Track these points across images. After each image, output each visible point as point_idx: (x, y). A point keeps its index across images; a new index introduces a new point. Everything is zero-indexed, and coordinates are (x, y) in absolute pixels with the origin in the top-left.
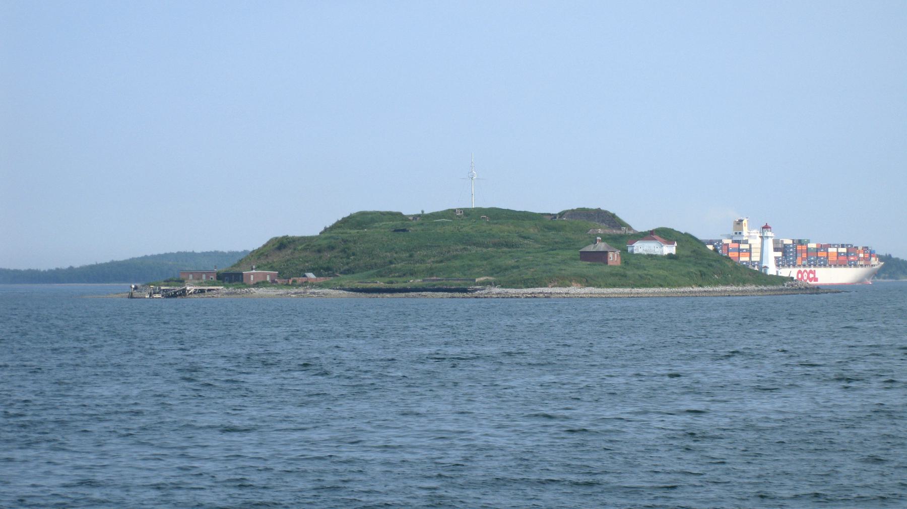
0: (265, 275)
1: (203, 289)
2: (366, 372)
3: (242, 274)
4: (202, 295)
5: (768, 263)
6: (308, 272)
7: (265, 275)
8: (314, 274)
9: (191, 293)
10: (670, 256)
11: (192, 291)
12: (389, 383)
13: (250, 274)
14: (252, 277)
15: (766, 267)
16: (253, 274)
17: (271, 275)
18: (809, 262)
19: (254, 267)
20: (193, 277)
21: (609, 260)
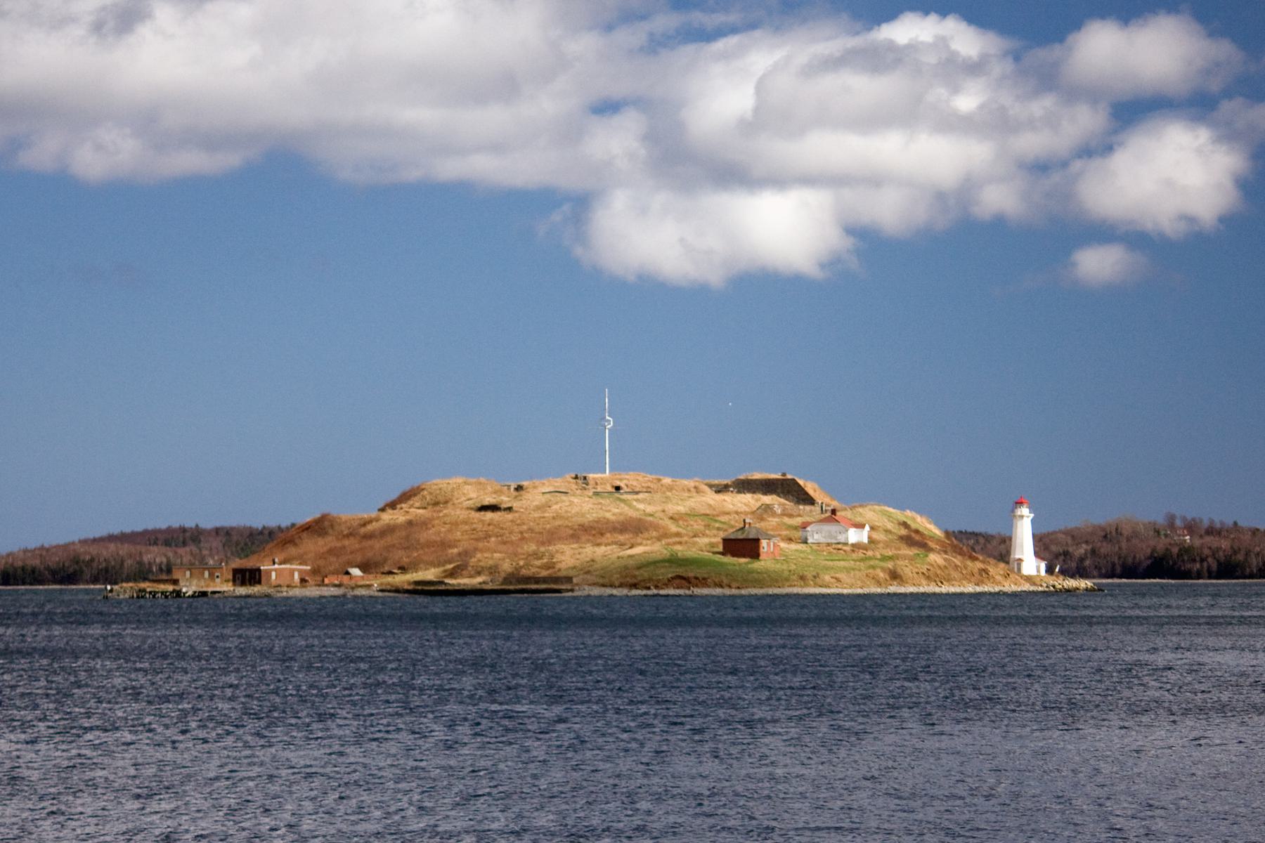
0: (292, 572)
1: (243, 584)
2: (422, 760)
3: (259, 570)
4: (205, 599)
5: (1023, 554)
6: (352, 567)
7: (292, 572)
8: (360, 570)
9: (189, 596)
10: (857, 547)
11: (190, 593)
12: (1158, 820)
13: (272, 570)
14: (274, 574)
15: (1020, 560)
16: (276, 570)
17: (300, 571)
18: (226, 655)
19: (276, 560)
20: (191, 574)
21: (761, 550)
